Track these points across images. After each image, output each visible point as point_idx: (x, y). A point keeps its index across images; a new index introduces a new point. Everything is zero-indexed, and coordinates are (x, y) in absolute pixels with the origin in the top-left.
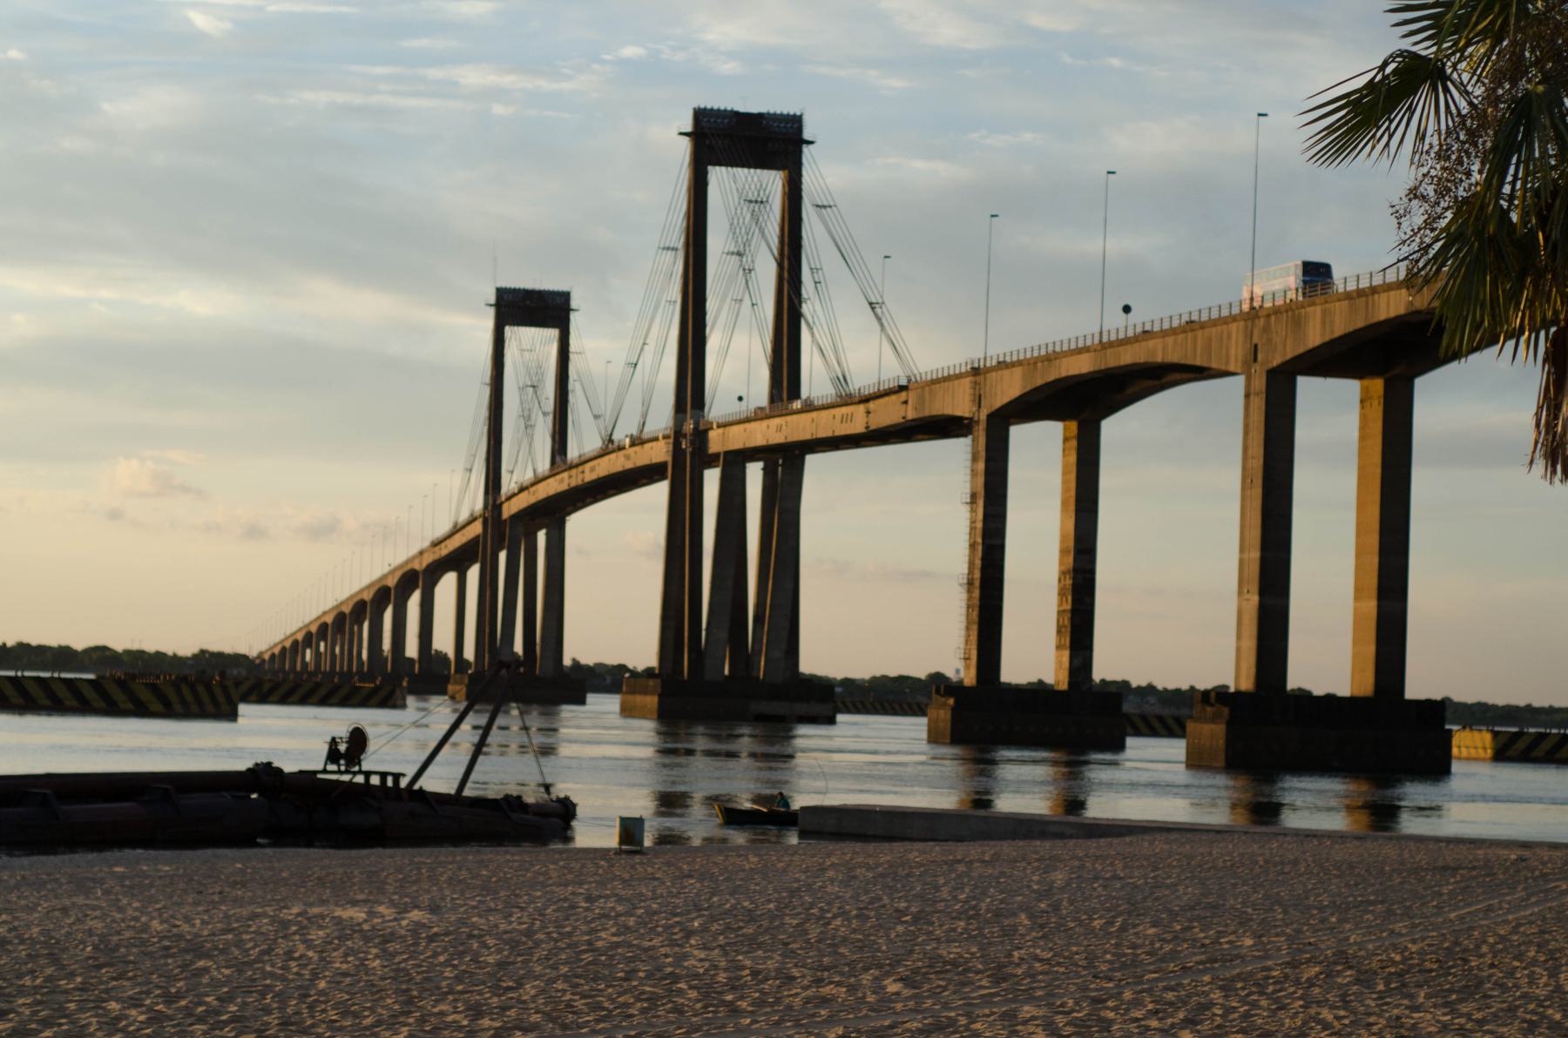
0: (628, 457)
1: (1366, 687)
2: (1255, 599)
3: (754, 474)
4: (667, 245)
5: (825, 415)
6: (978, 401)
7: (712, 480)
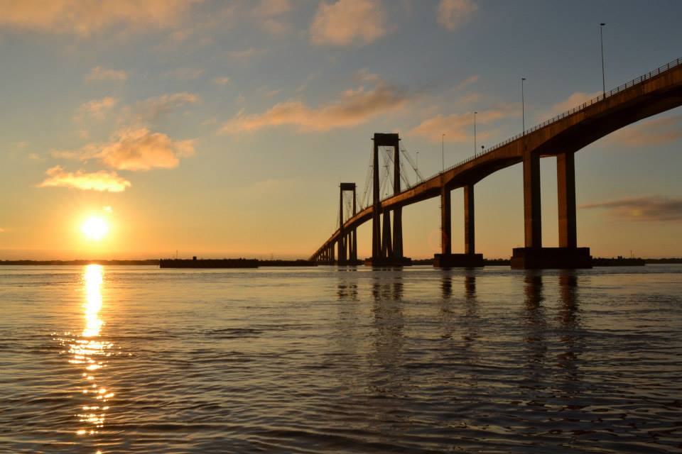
1: (565, 244)
2: (531, 220)
3: (392, 213)
5: (405, 194)
6: (442, 182)
7: (382, 216)
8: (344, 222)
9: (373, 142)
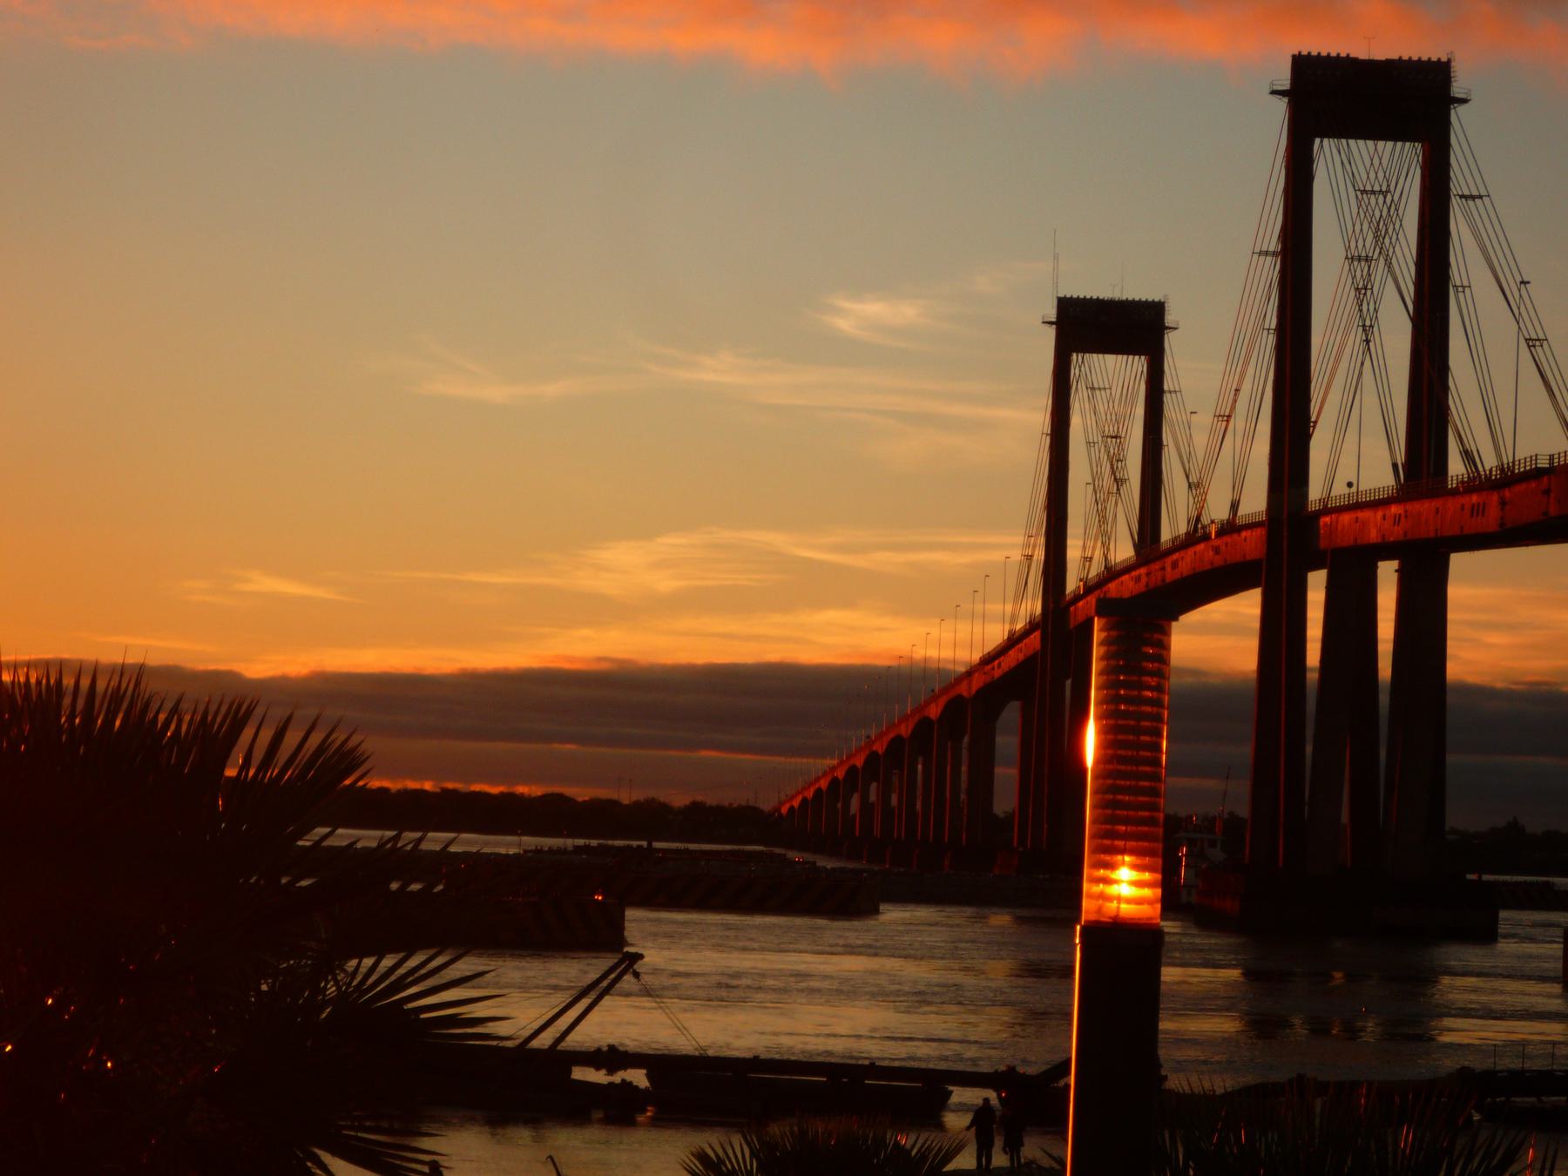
0: (1217, 550)
3: (1387, 575)
4: (1264, 249)
7: (1317, 588)
8: (1072, 584)
9: (1279, 109)
